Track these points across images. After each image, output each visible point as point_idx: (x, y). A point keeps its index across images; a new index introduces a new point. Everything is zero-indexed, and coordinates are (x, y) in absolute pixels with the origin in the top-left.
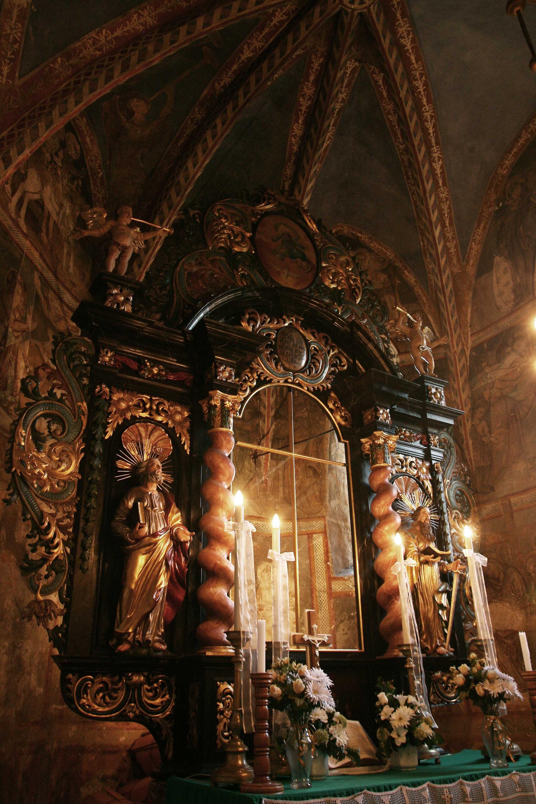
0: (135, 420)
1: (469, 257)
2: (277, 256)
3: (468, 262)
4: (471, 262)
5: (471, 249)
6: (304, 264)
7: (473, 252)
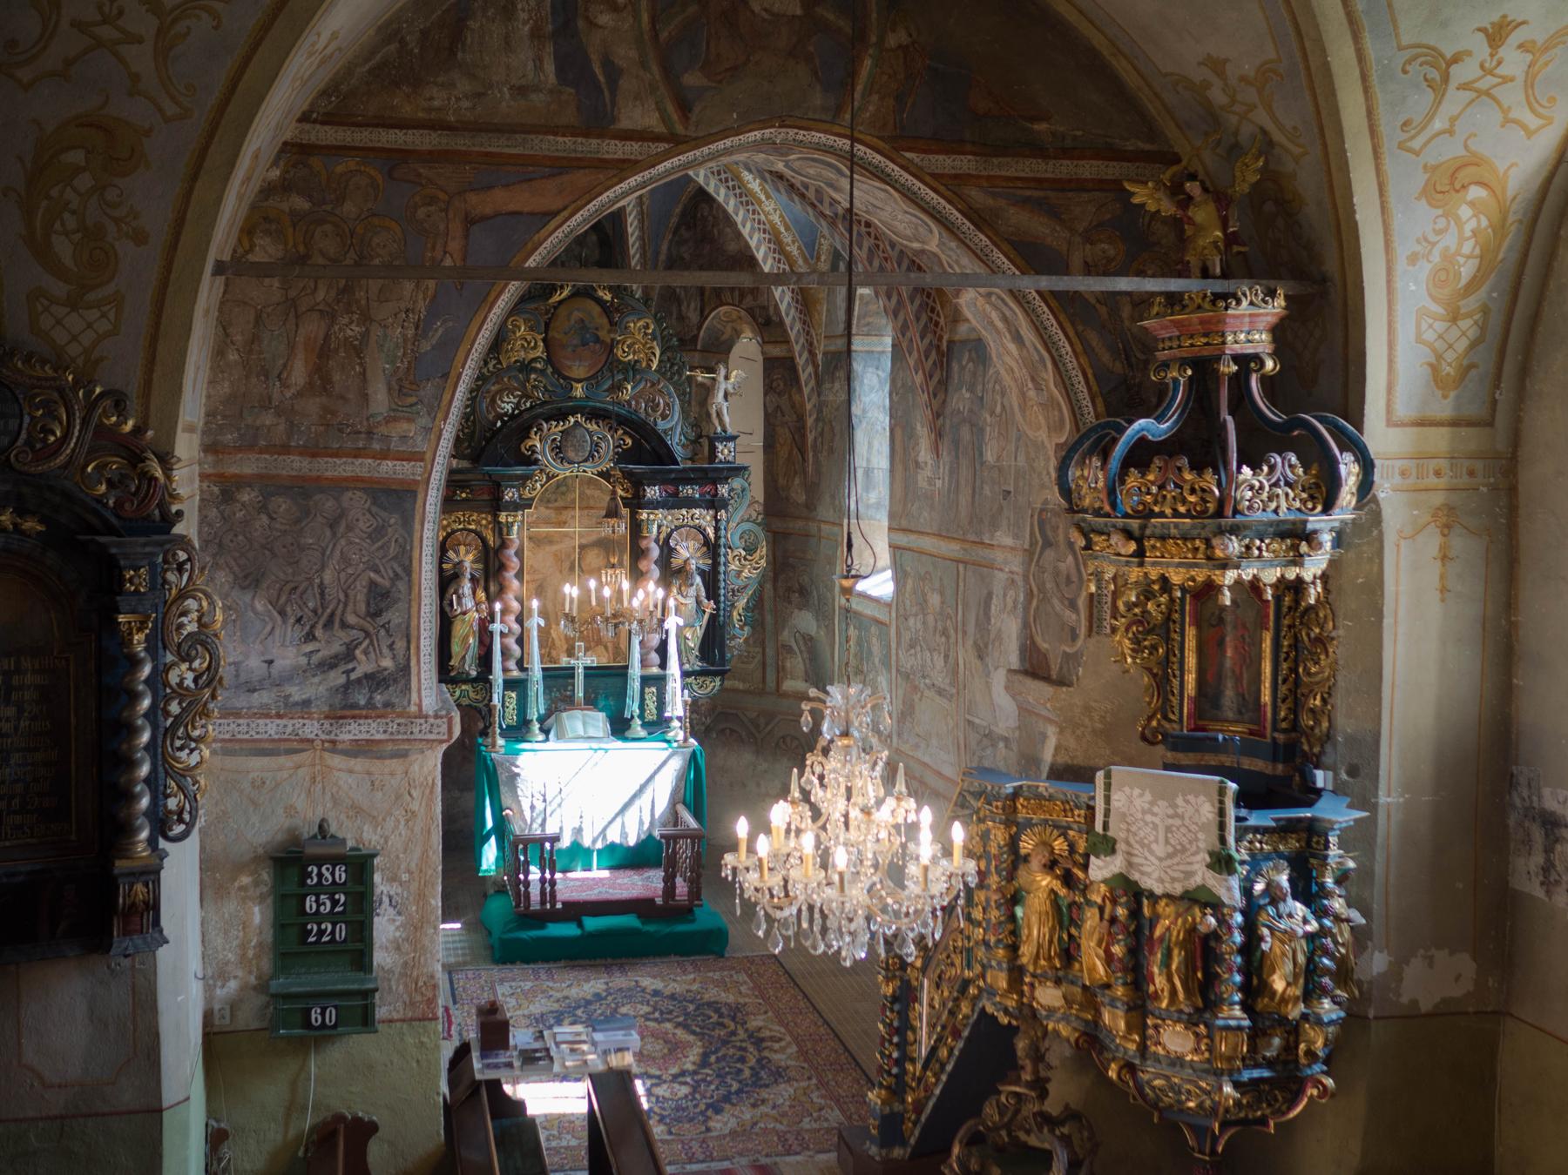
0: (454, 532)
1: (818, 253)
2: (570, 349)
3: (818, 259)
4: (823, 258)
5: (820, 244)
6: (598, 346)
7: (825, 248)
